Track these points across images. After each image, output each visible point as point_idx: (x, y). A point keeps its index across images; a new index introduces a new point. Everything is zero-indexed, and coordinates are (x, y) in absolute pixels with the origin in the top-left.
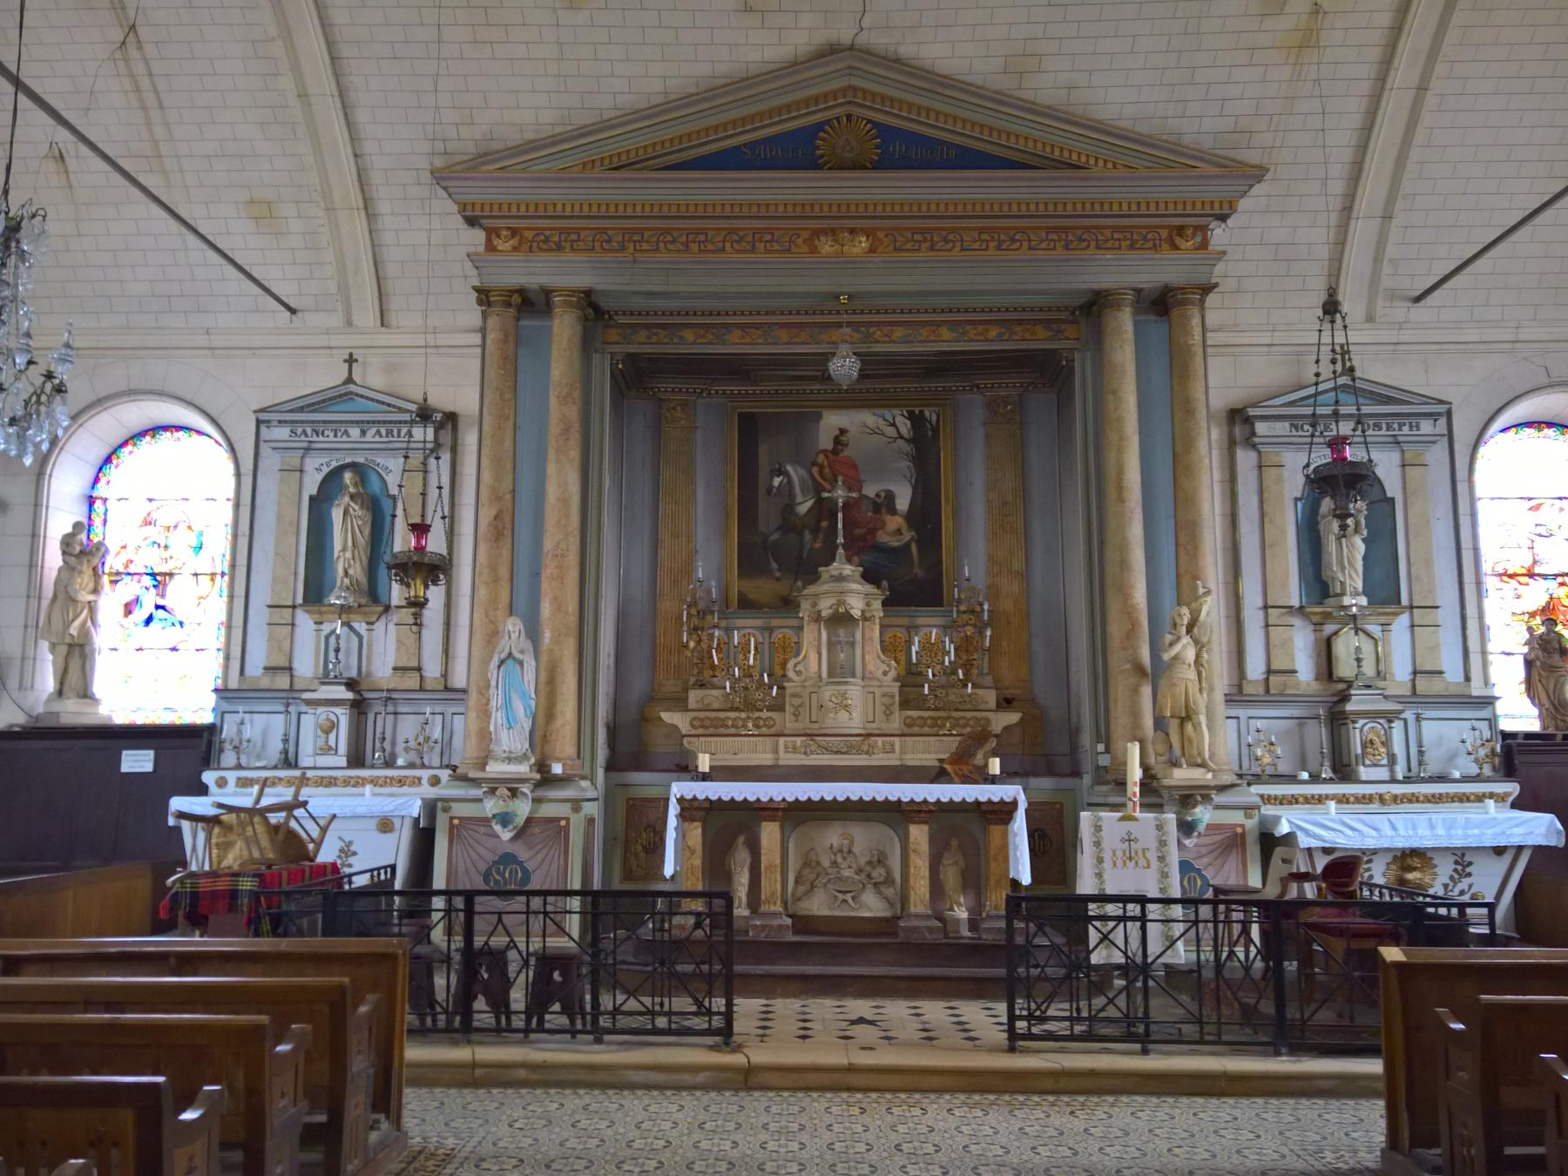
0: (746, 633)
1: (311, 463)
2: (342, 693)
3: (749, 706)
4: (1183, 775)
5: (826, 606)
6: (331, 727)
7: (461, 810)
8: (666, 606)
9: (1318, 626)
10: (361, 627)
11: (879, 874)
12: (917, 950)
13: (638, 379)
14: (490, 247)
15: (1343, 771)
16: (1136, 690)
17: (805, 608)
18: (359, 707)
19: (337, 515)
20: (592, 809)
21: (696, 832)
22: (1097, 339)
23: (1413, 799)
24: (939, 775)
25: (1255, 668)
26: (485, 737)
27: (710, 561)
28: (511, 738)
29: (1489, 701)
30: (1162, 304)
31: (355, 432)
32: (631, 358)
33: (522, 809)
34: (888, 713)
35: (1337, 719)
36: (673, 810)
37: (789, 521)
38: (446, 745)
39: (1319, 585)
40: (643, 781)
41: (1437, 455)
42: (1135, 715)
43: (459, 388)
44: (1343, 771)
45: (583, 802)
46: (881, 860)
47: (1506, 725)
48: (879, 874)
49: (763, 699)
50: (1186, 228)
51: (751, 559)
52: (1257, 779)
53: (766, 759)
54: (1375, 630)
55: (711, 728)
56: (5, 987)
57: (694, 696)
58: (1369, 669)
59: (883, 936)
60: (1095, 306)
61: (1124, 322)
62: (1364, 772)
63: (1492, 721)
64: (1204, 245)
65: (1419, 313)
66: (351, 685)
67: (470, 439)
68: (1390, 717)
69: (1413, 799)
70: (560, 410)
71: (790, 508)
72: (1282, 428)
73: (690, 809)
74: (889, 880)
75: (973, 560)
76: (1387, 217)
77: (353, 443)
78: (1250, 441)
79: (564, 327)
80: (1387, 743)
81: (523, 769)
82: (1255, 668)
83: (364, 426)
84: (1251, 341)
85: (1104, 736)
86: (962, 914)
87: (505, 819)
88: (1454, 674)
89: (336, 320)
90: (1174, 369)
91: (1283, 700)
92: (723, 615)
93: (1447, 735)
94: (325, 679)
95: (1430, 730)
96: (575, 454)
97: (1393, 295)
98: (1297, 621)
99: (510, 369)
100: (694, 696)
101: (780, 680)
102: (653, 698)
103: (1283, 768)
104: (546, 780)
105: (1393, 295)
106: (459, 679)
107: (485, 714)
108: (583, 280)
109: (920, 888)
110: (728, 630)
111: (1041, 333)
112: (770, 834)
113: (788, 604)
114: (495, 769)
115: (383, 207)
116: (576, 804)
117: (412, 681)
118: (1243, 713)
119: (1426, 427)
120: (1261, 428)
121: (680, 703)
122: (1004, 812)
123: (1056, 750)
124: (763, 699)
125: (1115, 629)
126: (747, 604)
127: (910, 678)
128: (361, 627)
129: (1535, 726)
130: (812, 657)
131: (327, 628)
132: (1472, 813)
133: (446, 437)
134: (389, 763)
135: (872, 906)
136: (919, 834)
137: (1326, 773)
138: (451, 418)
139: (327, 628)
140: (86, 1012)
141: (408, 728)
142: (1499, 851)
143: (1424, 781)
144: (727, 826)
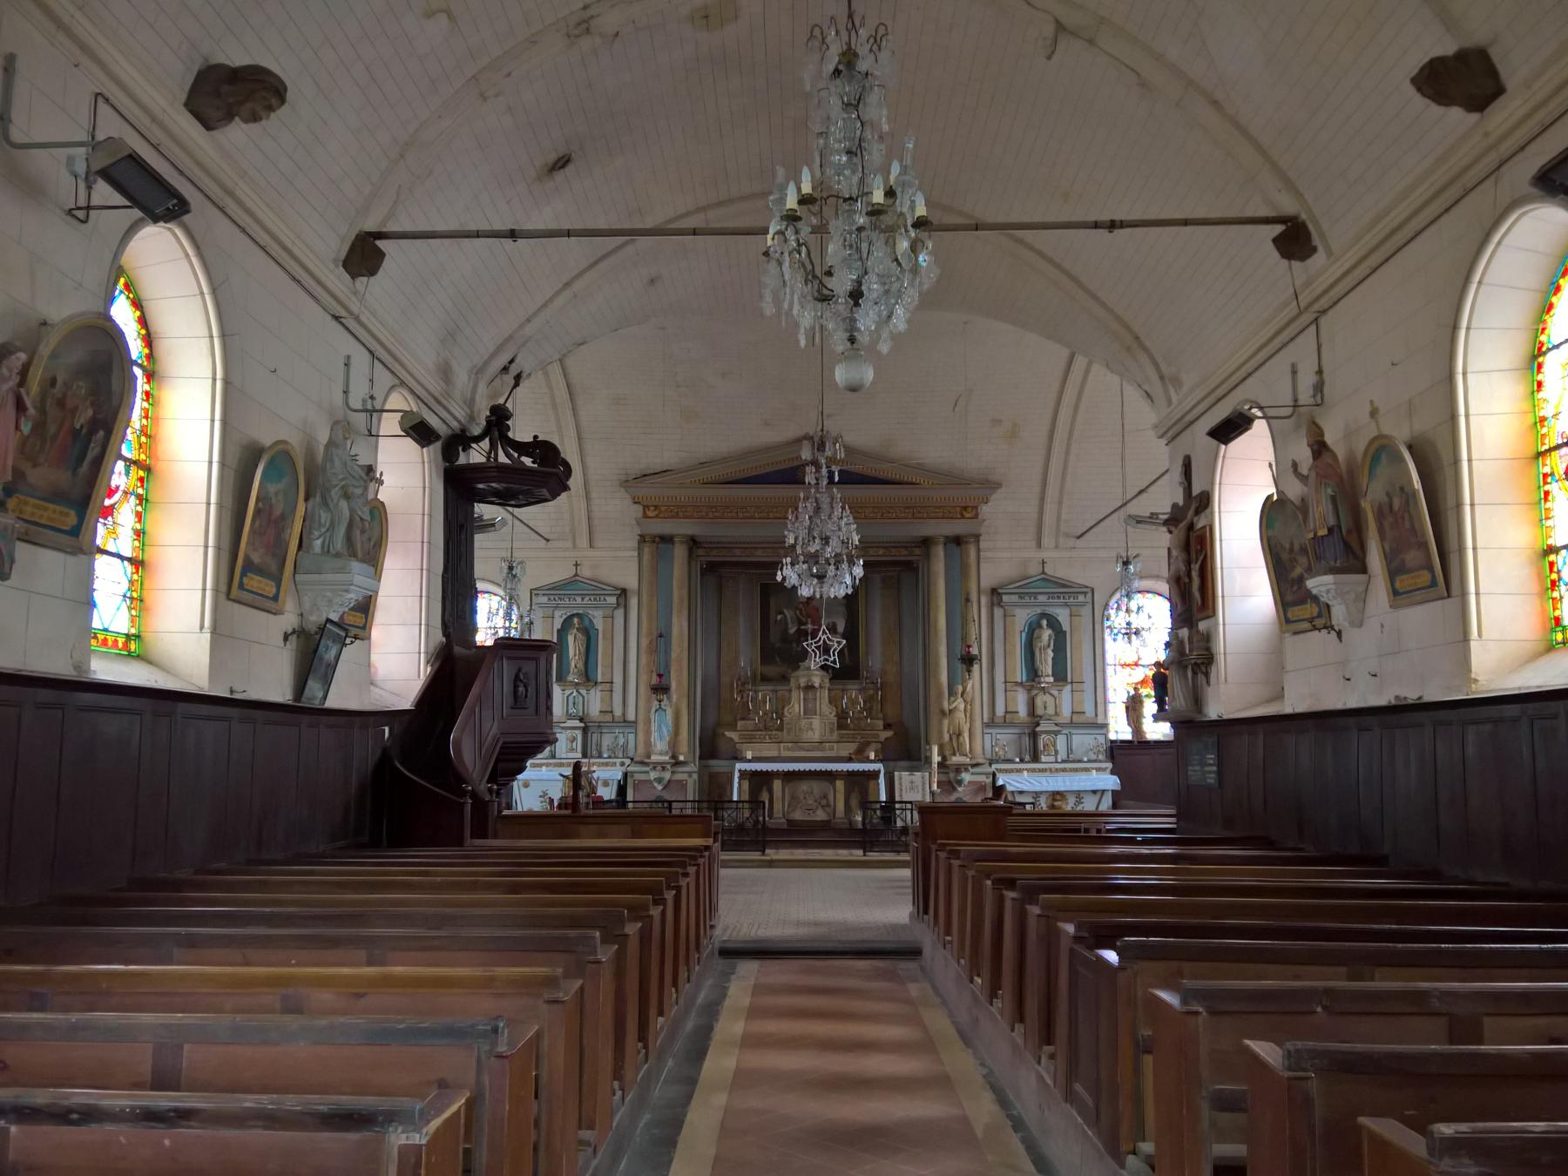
0: (764, 693)
1: (557, 613)
2: (577, 723)
3: (766, 729)
4: (957, 759)
5: (803, 682)
6: (574, 739)
7: (638, 777)
8: (725, 679)
9: (1029, 691)
10: (584, 692)
11: (824, 802)
12: (840, 832)
13: (711, 568)
14: (645, 516)
15: (1035, 758)
16: (940, 723)
17: (793, 682)
18: (585, 730)
19: (571, 639)
20: (695, 776)
21: (746, 784)
22: (927, 556)
23: (1064, 770)
24: (850, 760)
25: (1000, 711)
26: (648, 744)
27: (746, 657)
28: (660, 744)
29: (1105, 726)
30: (957, 541)
31: (579, 599)
32: (708, 563)
33: (667, 776)
34: (832, 731)
35: (1034, 736)
36: (737, 775)
37: (785, 637)
38: (625, 747)
39: (1033, 673)
40: (718, 765)
41: (1086, 611)
42: (940, 732)
43: (626, 574)
44: (1035, 758)
45: (689, 775)
46: (825, 797)
47: (1112, 736)
48: (824, 802)
49: (774, 725)
50: (968, 510)
51: (767, 654)
52: (997, 762)
53: (775, 754)
54: (1055, 693)
55: (750, 739)
56: (3, 973)
57: (740, 724)
58: (1051, 711)
59: (825, 826)
60: (926, 543)
61: (939, 552)
62: (1043, 758)
63: (1106, 735)
64: (976, 516)
65: (1079, 543)
66: (581, 720)
67: (633, 602)
68: (1056, 733)
69: (1064, 770)
70: (678, 591)
71: (786, 629)
72: (1015, 598)
73: (743, 774)
74: (828, 805)
75: (875, 658)
76: (1060, 503)
77: (578, 604)
78: (1000, 604)
79: (680, 552)
80: (1054, 745)
81: (667, 758)
82: (1000, 711)
83: (583, 596)
84: (998, 561)
85: (928, 742)
86: (859, 819)
87: (659, 780)
88: (1090, 713)
89: (569, 544)
90: (959, 574)
91: (1012, 725)
92: (754, 684)
93: (1084, 741)
94: (570, 717)
95: (1077, 740)
96: (685, 612)
97: (1067, 535)
98: (1020, 689)
99: (656, 574)
100: (740, 724)
101: (781, 716)
102: (718, 724)
103: (1009, 756)
104: (678, 763)
105: (1067, 535)
106: (631, 716)
107: (648, 733)
108: (690, 532)
109: (841, 806)
110: (756, 692)
111: (904, 552)
112: (777, 785)
113: (784, 679)
114: (654, 758)
115: (594, 495)
116: (690, 774)
117: (608, 718)
118: (994, 731)
119: (1081, 598)
120: (1005, 598)
121: (733, 727)
122: (875, 775)
123: (906, 749)
124: (774, 725)
125: (933, 694)
126: (765, 679)
127: (842, 716)
128: (584, 692)
129: (1129, 737)
130: (796, 706)
131: (568, 692)
132: (1083, 776)
133: (622, 601)
134: (600, 756)
135: (820, 815)
136: (840, 784)
137: (1027, 758)
138: (624, 591)
139: (568, 692)
140: (31, 1009)
141: (607, 740)
142: (1094, 792)
143: (1072, 762)
144: (759, 781)
